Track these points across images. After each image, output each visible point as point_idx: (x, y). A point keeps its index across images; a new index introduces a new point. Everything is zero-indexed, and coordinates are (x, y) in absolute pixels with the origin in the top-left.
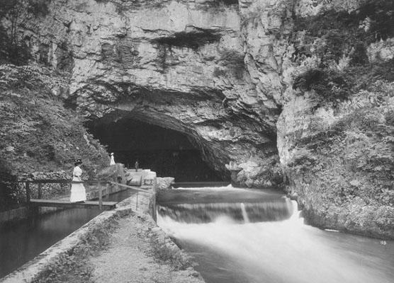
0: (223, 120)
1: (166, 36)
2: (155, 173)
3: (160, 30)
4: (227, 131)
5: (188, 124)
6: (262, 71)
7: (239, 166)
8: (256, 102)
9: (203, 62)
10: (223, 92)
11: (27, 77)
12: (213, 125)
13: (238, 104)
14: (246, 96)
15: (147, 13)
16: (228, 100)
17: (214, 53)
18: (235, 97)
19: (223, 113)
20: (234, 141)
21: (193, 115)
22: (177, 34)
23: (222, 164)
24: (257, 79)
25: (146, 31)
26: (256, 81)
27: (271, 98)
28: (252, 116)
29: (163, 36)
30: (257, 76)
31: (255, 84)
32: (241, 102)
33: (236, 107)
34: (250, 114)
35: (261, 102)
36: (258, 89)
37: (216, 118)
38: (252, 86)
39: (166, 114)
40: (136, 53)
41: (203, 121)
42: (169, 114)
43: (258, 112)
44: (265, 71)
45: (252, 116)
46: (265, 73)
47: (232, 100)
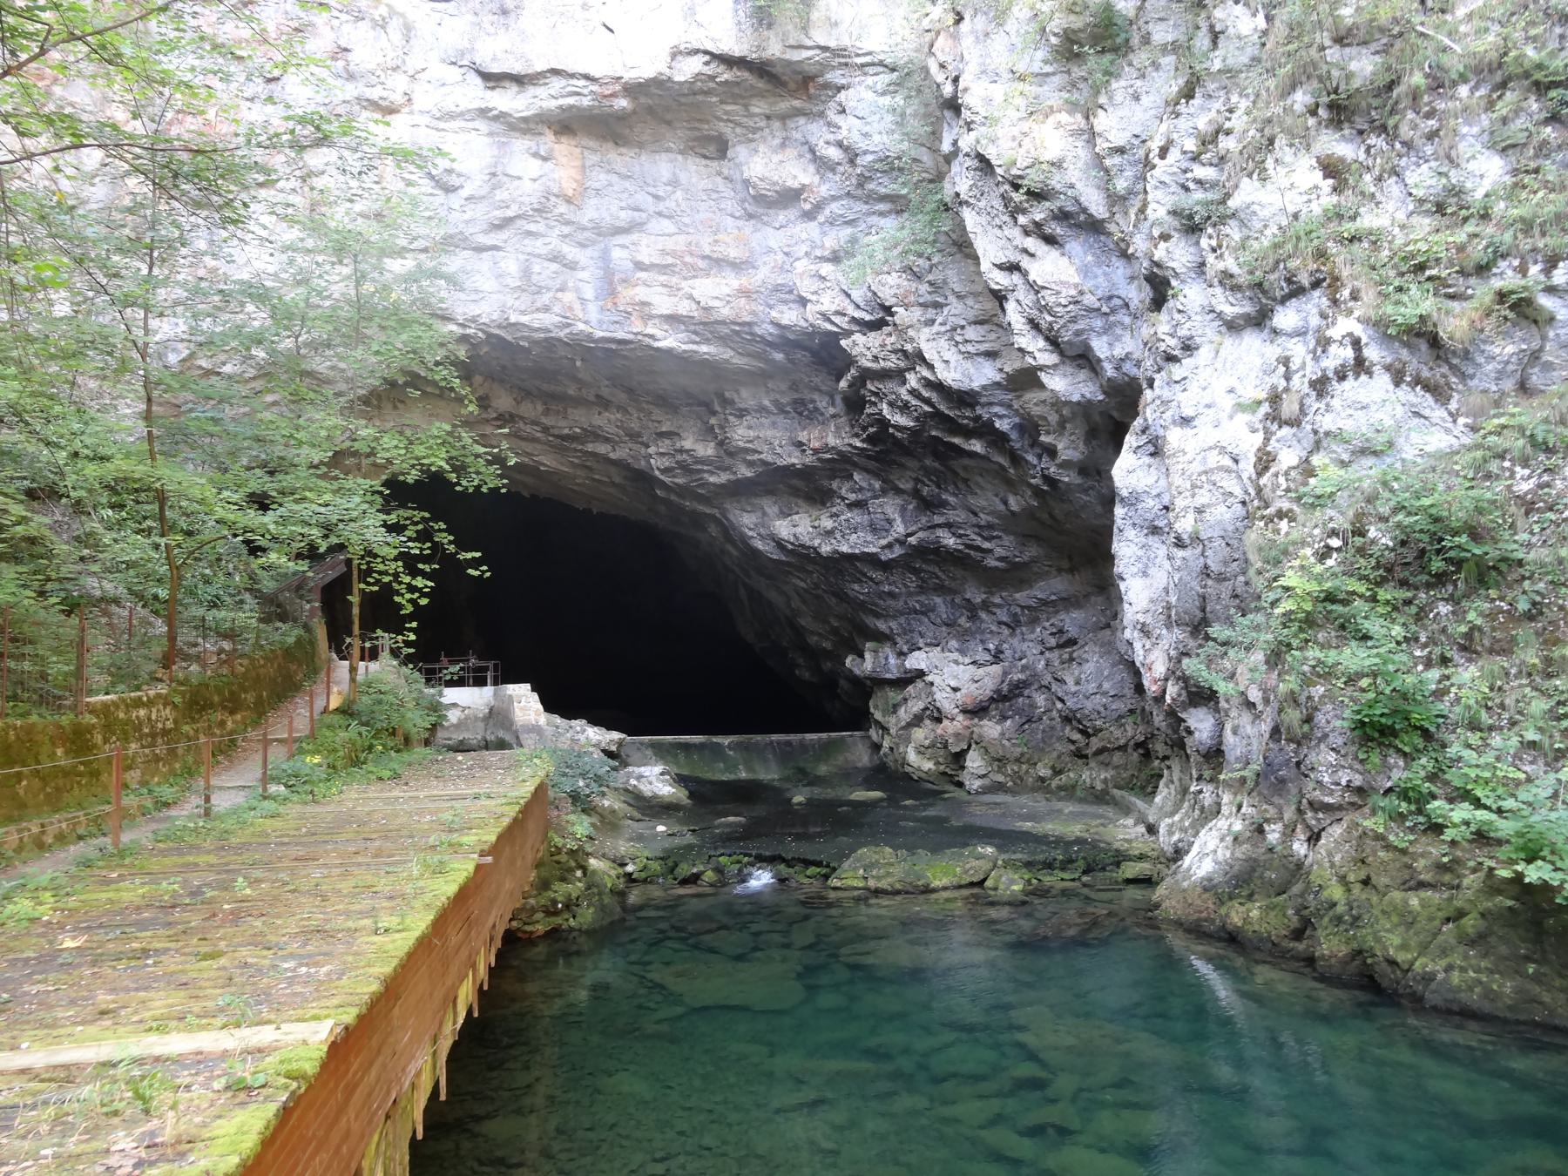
0: (841, 465)
1: (586, 102)
2: (528, 686)
3: (555, 72)
4: (856, 517)
5: (682, 491)
6: (1036, 230)
7: (908, 664)
8: (998, 377)
9: (750, 216)
10: (843, 343)
11: (933, 610)
12: (795, 492)
13: (913, 392)
14: (951, 355)
15: (407, 208)
16: (866, 375)
17: (797, 173)
18: (893, 362)
19: (836, 436)
20: (886, 556)
21: (707, 450)
22: (633, 89)
23: (828, 654)
24: (1012, 268)
25: (493, 79)
26: (999, 280)
27: (1083, 358)
28: (977, 446)
29: (571, 101)
30: (1014, 257)
31: (1000, 297)
32: (929, 384)
33: (905, 408)
34: (968, 434)
35: (1027, 379)
36: (1014, 315)
37: (809, 459)
38: (974, 308)
39: (590, 447)
40: (454, 180)
41: (748, 473)
42: (602, 449)
43: (1002, 425)
44: (1057, 229)
45: (977, 446)
46: (1050, 240)
47: (884, 375)
